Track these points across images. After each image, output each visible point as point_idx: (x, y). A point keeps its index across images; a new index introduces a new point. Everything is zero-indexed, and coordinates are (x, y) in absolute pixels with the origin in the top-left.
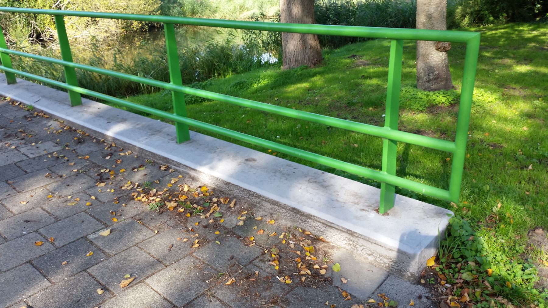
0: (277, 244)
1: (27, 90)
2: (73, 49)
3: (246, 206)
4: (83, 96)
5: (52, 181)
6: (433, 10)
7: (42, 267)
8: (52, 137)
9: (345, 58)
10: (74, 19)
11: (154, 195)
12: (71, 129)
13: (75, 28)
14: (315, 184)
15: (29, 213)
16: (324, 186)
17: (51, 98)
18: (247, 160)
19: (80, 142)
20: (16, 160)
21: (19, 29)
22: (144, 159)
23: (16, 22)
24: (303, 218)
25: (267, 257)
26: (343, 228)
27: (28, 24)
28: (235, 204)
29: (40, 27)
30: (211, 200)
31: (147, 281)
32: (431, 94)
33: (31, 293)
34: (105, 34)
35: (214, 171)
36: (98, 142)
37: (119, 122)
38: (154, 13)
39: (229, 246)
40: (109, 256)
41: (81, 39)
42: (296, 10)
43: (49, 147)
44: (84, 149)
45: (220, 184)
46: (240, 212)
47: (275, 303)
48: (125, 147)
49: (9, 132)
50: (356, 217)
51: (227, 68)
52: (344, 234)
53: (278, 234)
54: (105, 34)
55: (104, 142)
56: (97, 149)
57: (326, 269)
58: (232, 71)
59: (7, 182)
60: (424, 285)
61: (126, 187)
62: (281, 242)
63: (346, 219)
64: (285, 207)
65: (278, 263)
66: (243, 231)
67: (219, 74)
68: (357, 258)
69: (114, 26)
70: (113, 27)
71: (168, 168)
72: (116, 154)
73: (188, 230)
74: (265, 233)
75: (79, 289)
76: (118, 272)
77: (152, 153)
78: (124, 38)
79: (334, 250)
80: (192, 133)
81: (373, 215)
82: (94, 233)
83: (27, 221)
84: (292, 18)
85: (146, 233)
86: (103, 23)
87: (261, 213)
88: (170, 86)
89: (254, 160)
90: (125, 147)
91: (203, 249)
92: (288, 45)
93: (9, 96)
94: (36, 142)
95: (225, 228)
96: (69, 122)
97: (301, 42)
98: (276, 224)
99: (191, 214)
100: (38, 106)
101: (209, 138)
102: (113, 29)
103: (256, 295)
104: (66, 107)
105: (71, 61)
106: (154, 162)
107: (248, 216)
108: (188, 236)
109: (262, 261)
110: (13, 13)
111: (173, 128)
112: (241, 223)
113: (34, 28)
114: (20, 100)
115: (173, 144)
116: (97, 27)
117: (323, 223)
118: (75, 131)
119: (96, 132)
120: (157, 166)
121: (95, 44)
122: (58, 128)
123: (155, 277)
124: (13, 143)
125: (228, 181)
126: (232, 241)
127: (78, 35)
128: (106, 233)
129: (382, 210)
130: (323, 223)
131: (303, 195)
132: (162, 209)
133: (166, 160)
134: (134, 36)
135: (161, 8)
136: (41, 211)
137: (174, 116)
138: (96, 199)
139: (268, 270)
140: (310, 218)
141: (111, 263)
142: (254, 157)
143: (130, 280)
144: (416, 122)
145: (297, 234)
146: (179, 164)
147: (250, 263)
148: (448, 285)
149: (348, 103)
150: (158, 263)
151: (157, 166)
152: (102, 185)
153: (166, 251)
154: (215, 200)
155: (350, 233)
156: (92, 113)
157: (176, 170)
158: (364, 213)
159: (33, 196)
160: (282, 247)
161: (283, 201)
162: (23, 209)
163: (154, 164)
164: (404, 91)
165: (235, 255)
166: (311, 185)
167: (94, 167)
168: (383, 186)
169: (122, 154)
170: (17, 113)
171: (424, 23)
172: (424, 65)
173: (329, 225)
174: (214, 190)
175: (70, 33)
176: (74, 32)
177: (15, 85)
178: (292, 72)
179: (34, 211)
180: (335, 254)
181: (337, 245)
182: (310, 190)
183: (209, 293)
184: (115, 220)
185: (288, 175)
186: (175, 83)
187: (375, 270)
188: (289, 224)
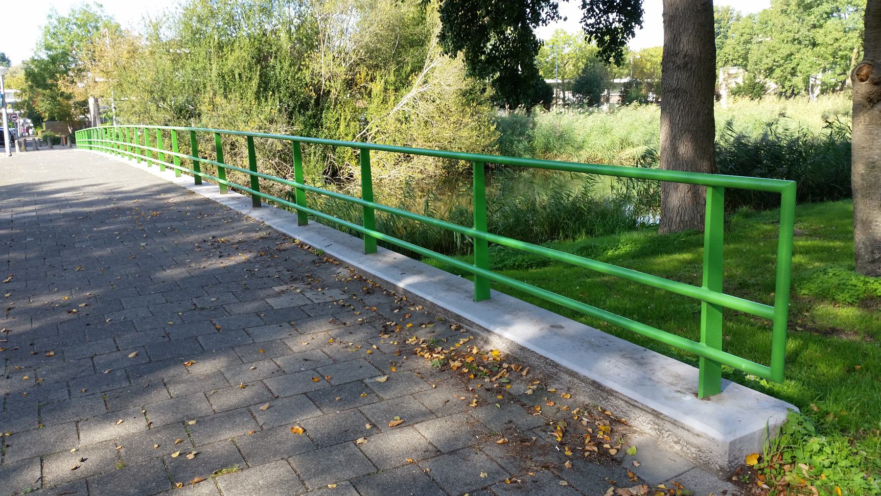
0: (568, 420)
1: (319, 233)
2: (375, 190)
3: (540, 376)
4: (381, 243)
5: (335, 327)
6: (876, 157)
7: (315, 399)
8: (340, 285)
9: (765, 223)
10: (381, 154)
11: (439, 353)
12: (362, 278)
13: (381, 165)
14: (628, 360)
15: (308, 353)
16: (641, 363)
17: (343, 244)
18: (552, 326)
19: (369, 292)
20: (300, 303)
21: (312, 164)
22: (433, 316)
23: (310, 155)
24: (605, 395)
25: (552, 428)
26: (647, 407)
27: (325, 158)
28: (528, 373)
29: (337, 161)
30: (501, 365)
31: (416, 426)
32: (872, 281)
33: (305, 418)
34: (420, 176)
35: (511, 333)
36: (388, 294)
37: (414, 274)
38: (490, 148)
39: (510, 412)
40: (382, 400)
41: (387, 181)
42: (685, 149)
43: (336, 294)
44: (372, 300)
45: (515, 350)
46: (531, 381)
47: (547, 468)
48: (416, 300)
49: (295, 276)
50: (667, 398)
51: (579, 229)
52: (648, 415)
53: (570, 409)
54: (420, 176)
55: (394, 294)
56: (386, 301)
57: (618, 450)
58: (587, 233)
59: (289, 323)
60: (735, 483)
61: (412, 341)
62: (572, 418)
63: (654, 398)
64: (584, 380)
65: (561, 435)
66: (530, 400)
67: (567, 237)
68: (662, 446)
69: (433, 165)
70: (431, 166)
71: (459, 328)
72: (406, 308)
73: (468, 390)
74: (556, 406)
75: (349, 422)
76: (389, 413)
77: (445, 310)
78: (444, 182)
79: (636, 435)
80: (493, 292)
81: (689, 398)
82: (371, 378)
83: (306, 360)
84: (677, 159)
85: (424, 386)
86: (417, 161)
87: (556, 386)
88: (472, 231)
89: (561, 327)
90: (416, 301)
91: (479, 409)
92: (669, 199)
93: (299, 238)
94: (323, 289)
95: (510, 394)
96: (360, 270)
97: (690, 194)
98: (572, 400)
99: (475, 376)
100: (328, 251)
101: (512, 300)
102: (431, 169)
103: (527, 457)
104: (358, 254)
105: (371, 200)
106: (446, 320)
107: (540, 387)
108: (467, 395)
109: (545, 431)
110: (308, 143)
111: (471, 285)
112: (529, 392)
113: (331, 162)
114: (310, 243)
115: (470, 302)
116: (410, 165)
117: (626, 402)
118: (365, 280)
119: (387, 283)
120: (448, 324)
121: (408, 189)
122: (347, 276)
123: (424, 424)
124: (298, 288)
125: (524, 345)
126: (515, 408)
127: (385, 175)
128: (383, 379)
129: (701, 394)
130: (626, 402)
131: (613, 371)
132: (445, 364)
133: (458, 318)
134: (457, 180)
135: (501, 141)
136: (321, 353)
137: (474, 268)
138: (378, 348)
139: (549, 440)
140: (612, 395)
141: (384, 405)
142: (562, 324)
143: (400, 422)
144: (836, 316)
145: (595, 412)
146: (472, 324)
147: (529, 430)
148: (765, 486)
149: (740, 284)
150: (430, 414)
151: (448, 324)
152: (386, 336)
153: (441, 406)
154: (505, 365)
155: (656, 414)
156: (386, 262)
157: (468, 331)
158: (679, 395)
159: (314, 339)
160: (573, 422)
161: (583, 372)
162: (303, 349)
163: (444, 322)
164: (831, 274)
165: (514, 420)
166: (624, 360)
167: (380, 319)
168: (702, 362)
169: (412, 309)
170: (306, 257)
171: (862, 174)
172: (864, 237)
173: (632, 404)
174: (507, 355)
175: (374, 170)
176: (379, 170)
177: (306, 227)
178: (672, 237)
179: (315, 352)
180: (635, 439)
181: (642, 428)
182: (620, 364)
183: (477, 447)
184: (394, 370)
185: (599, 347)
186: (478, 229)
187: (678, 460)
188: (587, 401)
